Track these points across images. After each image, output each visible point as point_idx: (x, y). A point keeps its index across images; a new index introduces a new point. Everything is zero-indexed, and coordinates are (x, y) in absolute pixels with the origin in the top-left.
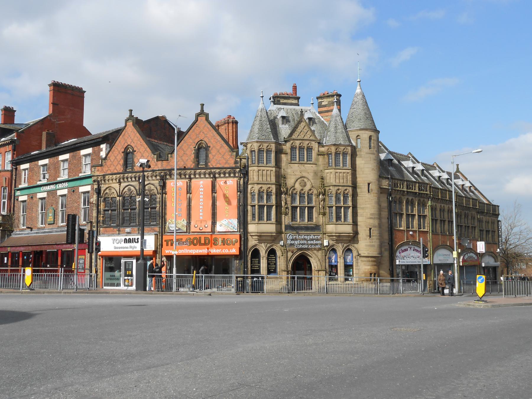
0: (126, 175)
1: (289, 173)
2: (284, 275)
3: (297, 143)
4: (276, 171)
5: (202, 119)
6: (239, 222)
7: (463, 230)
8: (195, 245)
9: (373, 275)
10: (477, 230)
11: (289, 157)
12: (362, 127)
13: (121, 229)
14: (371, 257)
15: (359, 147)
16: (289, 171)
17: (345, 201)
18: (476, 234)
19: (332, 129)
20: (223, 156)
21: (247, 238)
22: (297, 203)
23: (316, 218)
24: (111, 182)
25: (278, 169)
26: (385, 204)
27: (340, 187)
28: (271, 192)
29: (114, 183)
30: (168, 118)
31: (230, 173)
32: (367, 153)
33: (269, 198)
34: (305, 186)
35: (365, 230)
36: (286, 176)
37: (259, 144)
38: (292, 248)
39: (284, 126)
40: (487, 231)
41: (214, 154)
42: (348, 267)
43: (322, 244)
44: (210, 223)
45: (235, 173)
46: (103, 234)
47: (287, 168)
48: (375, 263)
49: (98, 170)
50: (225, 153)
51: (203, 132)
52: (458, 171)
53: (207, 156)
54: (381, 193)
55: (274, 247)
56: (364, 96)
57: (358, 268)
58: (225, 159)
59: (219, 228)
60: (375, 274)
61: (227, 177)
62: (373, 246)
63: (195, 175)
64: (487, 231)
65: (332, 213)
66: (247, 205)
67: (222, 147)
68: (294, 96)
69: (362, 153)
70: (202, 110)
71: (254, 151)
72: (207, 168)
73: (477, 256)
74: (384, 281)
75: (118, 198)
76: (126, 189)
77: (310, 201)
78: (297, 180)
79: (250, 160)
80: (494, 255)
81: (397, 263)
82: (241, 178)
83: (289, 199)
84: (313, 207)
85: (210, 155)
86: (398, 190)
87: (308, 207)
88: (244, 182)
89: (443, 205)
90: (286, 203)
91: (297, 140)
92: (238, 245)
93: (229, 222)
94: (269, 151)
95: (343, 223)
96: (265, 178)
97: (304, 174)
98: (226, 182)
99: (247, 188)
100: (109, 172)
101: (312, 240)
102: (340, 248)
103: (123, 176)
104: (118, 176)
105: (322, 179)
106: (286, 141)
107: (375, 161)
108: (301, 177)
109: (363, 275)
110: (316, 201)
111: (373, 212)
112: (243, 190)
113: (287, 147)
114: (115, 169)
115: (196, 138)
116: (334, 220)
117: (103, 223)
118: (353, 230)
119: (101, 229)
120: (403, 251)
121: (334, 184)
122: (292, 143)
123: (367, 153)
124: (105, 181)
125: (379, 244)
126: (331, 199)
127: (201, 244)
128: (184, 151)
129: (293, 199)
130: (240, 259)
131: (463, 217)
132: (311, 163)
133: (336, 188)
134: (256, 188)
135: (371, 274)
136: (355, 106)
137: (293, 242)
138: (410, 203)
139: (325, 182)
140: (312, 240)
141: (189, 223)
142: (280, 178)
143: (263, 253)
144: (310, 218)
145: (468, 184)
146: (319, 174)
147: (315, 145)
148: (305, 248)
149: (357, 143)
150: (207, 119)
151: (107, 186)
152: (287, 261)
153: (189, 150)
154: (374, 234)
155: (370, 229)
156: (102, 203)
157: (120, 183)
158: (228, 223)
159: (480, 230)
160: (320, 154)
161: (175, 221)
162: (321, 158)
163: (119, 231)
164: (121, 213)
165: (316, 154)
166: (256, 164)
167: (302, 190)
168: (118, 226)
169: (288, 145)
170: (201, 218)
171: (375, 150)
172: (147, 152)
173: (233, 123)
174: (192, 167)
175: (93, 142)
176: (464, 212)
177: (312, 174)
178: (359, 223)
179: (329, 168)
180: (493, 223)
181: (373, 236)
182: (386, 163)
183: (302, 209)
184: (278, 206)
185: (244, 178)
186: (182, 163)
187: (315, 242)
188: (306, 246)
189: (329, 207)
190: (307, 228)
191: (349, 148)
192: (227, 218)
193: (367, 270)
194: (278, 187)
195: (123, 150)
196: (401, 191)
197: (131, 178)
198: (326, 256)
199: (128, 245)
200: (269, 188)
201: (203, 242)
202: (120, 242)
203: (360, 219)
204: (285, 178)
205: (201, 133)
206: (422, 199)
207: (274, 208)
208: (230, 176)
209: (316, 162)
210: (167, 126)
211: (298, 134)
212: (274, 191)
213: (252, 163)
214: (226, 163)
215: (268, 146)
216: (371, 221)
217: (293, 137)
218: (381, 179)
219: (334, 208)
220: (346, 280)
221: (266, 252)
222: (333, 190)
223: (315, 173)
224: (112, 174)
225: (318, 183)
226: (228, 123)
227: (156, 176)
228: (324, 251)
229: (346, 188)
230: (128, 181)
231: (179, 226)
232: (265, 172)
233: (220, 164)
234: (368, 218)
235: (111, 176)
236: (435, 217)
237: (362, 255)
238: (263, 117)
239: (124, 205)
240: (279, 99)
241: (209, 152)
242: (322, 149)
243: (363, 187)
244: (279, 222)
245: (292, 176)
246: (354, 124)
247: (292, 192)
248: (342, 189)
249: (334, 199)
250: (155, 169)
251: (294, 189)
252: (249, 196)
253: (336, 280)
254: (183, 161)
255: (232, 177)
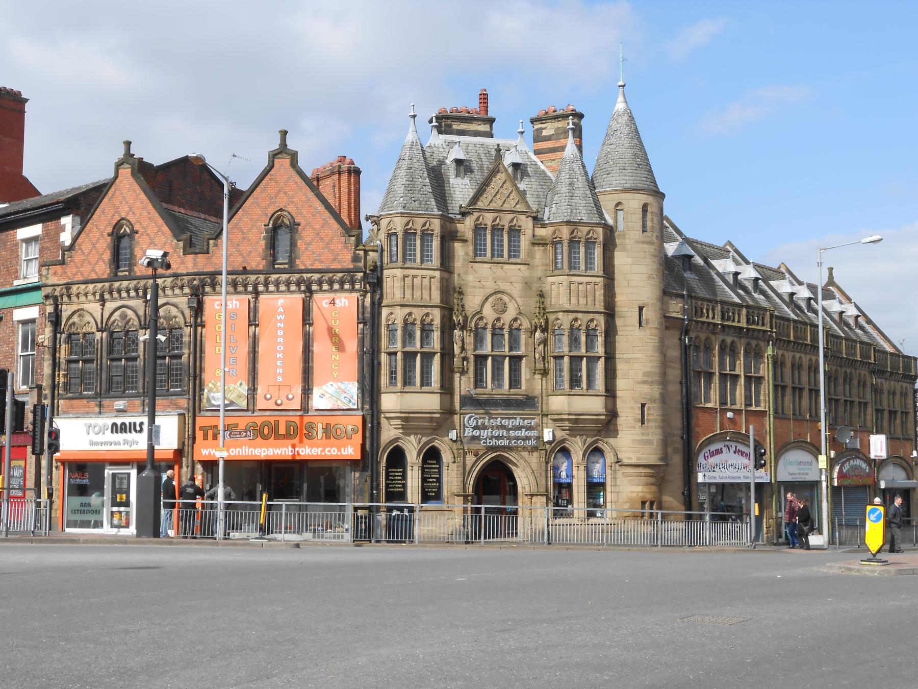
0: (117, 284)
1: (470, 284)
2: (458, 504)
3: (488, 218)
4: (442, 279)
5: (283, 163)
6: (362, 388)
7: (841, 409)
8: (265, 438)
9: (647, 505)
10: (869, 411)
11: (471, 248)
12: (628, 186)
13: (106, 402)
14: (645, 466)
15: (621, 227)
16: (470, 278)
17: (590, 345)
18: (869, 418)
19: (563, 189)
20: (328, 243)
21: (379, 424)
22: (487, 349)
23: (527, 380)
24: (83, 298)
25: (446, 275)
26: (675, 353)
27: (580, 315)
28: (430, 324)
29: (90, 302)
30: (28, 107)
31: (342, 283)
32: (637, 242)
33: (427, 336)
34: (504, 311)
35: (632, 408)
36: (464, 288)
37: (405, 220)
38: (474, 446)
39: (459, 180)
40: (902, 412)
41: (308, 239)
42: (595, 489)
43: (539, 438)
44: (298, 390)
45: (353, 283)
46: (65, 413)
47: (466, 273)
48: (653, 480)
49: (55, 274)
50: (332, 239)
51: (285, 193)
52: (831, 281)
53: (293, 244)
54: (667, 328)
55: (436, 444)
56: (631, 118)
57: (617, 489)
58: (331, 251)
59: (317, 402)
60: (652, 503)
61: (336, 291)
62: (649, 442)
63: (266, 285)
64: (892, 413)
65: (561, 370)
66: (379, 352)
67: (325, 224)
68: (482, 115)
69: (627, 241)
70: (283, 144)
71: (395, 234)
72: (292, 270)
73: (870, 465)
74: (672, 517)
75: (98, 335)
76: (116, 315)
77: (514, 343)
78: (487, 299)
79: (385, 254)
80: (905, 464)
81: (700, 479)
82: (366, 292)
83: (469, 340)
84: (520, 358)
85: (299, 243)
86: (703, 323)
87: (511, 357)
88: (373, 303)
89: (797, 355)
90: (463, 349)
91: (488, 211)
92: (358, 439)
93: (340, 388)
94: (426, 235)
95: (584, 391)
96: (417, 294)
97: (503, 286)
98: (333, 302)
99: (380, 314)
100: (80, 278)
101: (519, 428)
102: (577, 447)
103: (111, 286)
104: (100, 285)
105: (541, 295)
106: (464, 214)
107: (656, 260)
108: (496, 293)
109: (627, 506)
110: (527, 345)
111: (648, 369)
112: (370, 320)
113: (466, 227)
114: (93, 270)
115: (269, 205)
116: (566, 385)
117: (65, 390)
118: (606, 408)
119: (61, 402)
120: (712, 454)
121: (567, 307)
122: (478, 219)
123: (637, 242)
124: (69, 297)
125: (661, 437)
126: (560, 341)
127: (278, 437)
128: (243, 233)
129: (479, 341)
130: (364, 469)
131: (841, 381)
132: (518, 261)
133: (572, 316)
134: (399, 315)
135: (643, 503)
136: (613, 140)
137: (476, 433)
138: (728, 350)
139: (547, 303)
140: (519, 428)
141: (253, 390)
142: (450, 294)
143: (413, 456)
144: (515, 381)
145: (851, 311)
146: (535, 286)
147: (526, 223)
148: (504, 447)
149: (616, 220)
150: (294, 164)
151: (75, 308)
152: (465, 474)
153: (255, 230)
154: (651, 417)
155: (643, 406)
156: (63, 346)
157: (103, 301)
158: (336, 391)
159: (877, 410)
160: (537, 242)
161: (222, 386)
162: (538, 250)
163: (100, 406)
164: (104, 367)
165: (527, 243)
166: (400, 264)
167: (498, 319)
168: (98, 395)
169: (469, 221)
170: (280, 379)
171: (655, 234)
172: (163, 234)
173: (349, 172)
174: (261, 267)
175: (44, 210)
176: (843, 370)
177: (519, 286)
178: (619, 394)
179: (556, 272)
180: (904, 395)
181: (649, 421)
182: (678, 263)
183: (498, 362)
184: (447, 354)
185: (373, 292)
186: (240, 259)
187: (524, 433)
188: (505, 442)
189: (555, 358)
190: (508, 403)
191: (600, 231)
192: (336, 380)
193: (634, 495)
194: (446, 312)
195: (110, 230)
196: (709, 324)
197: (128, 291)
198: (547, 463)
199: (120, 437)
200: (427, 315)
201: (282, 431)
202: (102, 431)
203: (621, 384)
204: (461, 293)
205: (282, 194)
206: (754, 343)
207: (437, 360)
208: (342, 289)
209: (529, 261)
210: (206, 176)
211: (490, 198)
212: (437, 322)
213: (391, 261)
214: (334, 260)
215: (424, 225)
216: (646, 389)
217: (480, 205)
218: (666, 298)
219: (566, 359)
220: (591, 515)
221: (418, 455)
222: (565, 320)
223: (527, 284)
224: (86, 282)
225: (532, 305)
226: (340, 173)
227: (182, 288)
228: (543, 452)
229: (591, 316)
230: (121, 298)
231: (232, 396)
232: (417, 281)
233: (321, 262)
234: (639, 383)
235: (83, 286)
236: (799, 383)
237: (626, 461)
238: (415, 160)
239: (111, 350)
240: (449, 122)
241: (297, 236)
242: (541, 232)
243: (628, 314)
244: (447, 389)
245: (478, 290)
246: (609, 178)
247: (476, 325)
248: (584, 319)
249: (565, 339)
250: (180, 271)
251: (481, 318)
252: (384, 331)
253: (569, 515)
254: (241, 254)
255: (347, 290)
